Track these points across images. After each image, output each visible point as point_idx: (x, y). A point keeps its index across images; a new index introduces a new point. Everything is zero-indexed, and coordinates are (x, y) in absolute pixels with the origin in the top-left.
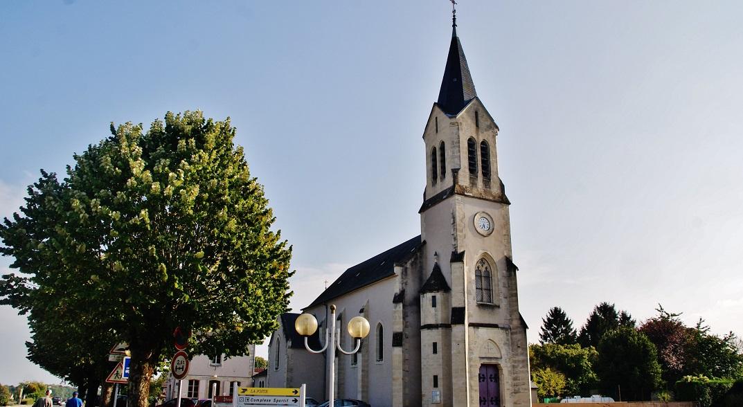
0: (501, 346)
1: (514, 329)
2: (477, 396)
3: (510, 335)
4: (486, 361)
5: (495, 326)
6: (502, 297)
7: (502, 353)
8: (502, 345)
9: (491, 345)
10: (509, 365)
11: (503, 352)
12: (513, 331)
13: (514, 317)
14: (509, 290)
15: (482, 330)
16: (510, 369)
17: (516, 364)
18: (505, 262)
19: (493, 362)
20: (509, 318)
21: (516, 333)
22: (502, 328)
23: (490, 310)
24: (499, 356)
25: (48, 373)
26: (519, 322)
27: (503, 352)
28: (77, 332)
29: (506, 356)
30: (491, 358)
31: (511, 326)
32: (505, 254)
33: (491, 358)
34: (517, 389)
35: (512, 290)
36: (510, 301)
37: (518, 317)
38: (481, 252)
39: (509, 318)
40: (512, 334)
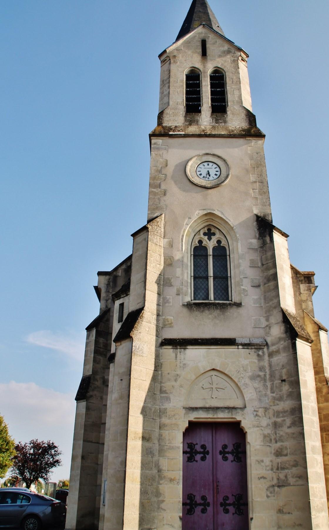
0: (244, 380)
1: (273, 345)
2: (102, 486)
3: (266, 357)
4: (193, 416)
5: (230, 342)
6: (246, 285)
7: (247, 397)
8: (247, 381)
9: (218, 380)
10: (265, 422)
11: (250, 394)
12: (272, 348)
13: (273, 320)
14: (263, 271)
15: (192, 352)
16: (268, 431)
17: (279, 420)
18: (255, 223)
19: (222, 416)
20: (264, 323)
21: (278, 352)
22: (246, 345)
23: (217, 312)
24: (238, 403)
25: (96, 295)
26: (283, 328)
27: (250, 394)
28: (3, 464)
29: (256, 404)
30: (217, 408)
31: (269, 340)
32: (256, 211)
33: (216, 409)
34: (282, 476)
35: (268, 269)
36: (265, 292)
37: (280, 318)
38: (198, 213)
39: (264, 323)
40: (271, 355)
